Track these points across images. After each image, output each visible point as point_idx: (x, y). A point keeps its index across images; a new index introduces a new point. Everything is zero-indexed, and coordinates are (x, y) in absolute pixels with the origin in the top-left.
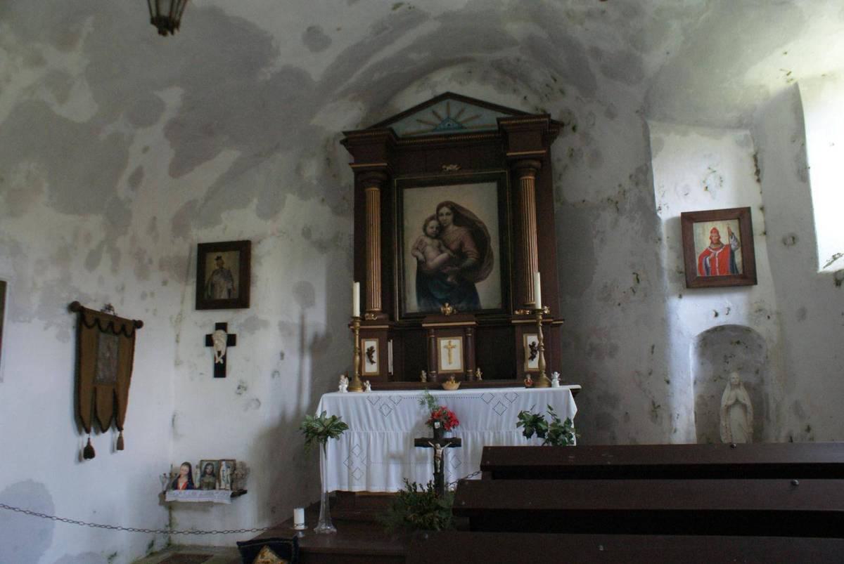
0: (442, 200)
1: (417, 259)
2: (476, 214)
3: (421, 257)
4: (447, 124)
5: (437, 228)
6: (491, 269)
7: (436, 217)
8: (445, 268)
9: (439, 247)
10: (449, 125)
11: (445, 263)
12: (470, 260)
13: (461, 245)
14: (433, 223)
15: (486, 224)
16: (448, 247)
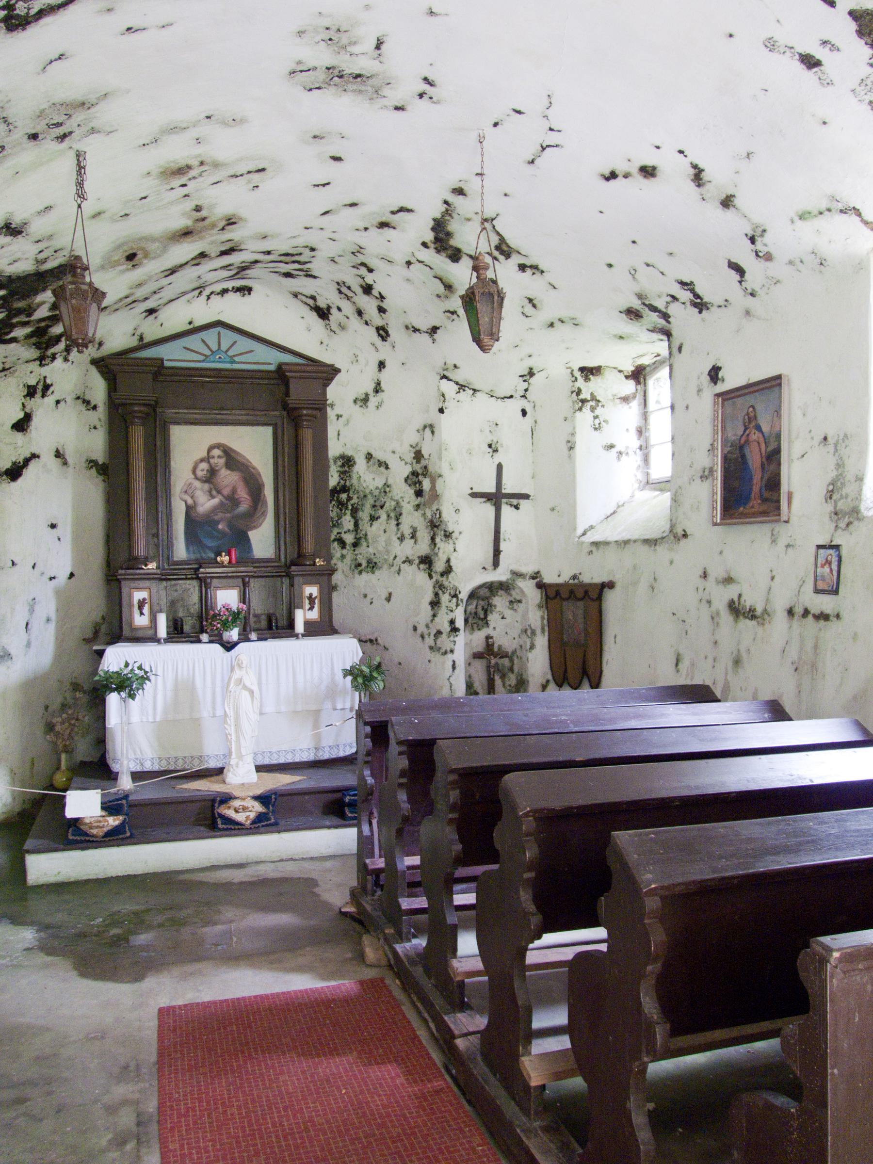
0: (214, 441)
1: (186, 503)
2: (248, 457)
3: (190, 501)
4: (217, 357)
7: (207, 459)
9: (210, 492)
10: (220, 358)
11: (214, 510)
12: (244, 507)
13: (234, 491)
14: (204, 466)
16: (219, 492)
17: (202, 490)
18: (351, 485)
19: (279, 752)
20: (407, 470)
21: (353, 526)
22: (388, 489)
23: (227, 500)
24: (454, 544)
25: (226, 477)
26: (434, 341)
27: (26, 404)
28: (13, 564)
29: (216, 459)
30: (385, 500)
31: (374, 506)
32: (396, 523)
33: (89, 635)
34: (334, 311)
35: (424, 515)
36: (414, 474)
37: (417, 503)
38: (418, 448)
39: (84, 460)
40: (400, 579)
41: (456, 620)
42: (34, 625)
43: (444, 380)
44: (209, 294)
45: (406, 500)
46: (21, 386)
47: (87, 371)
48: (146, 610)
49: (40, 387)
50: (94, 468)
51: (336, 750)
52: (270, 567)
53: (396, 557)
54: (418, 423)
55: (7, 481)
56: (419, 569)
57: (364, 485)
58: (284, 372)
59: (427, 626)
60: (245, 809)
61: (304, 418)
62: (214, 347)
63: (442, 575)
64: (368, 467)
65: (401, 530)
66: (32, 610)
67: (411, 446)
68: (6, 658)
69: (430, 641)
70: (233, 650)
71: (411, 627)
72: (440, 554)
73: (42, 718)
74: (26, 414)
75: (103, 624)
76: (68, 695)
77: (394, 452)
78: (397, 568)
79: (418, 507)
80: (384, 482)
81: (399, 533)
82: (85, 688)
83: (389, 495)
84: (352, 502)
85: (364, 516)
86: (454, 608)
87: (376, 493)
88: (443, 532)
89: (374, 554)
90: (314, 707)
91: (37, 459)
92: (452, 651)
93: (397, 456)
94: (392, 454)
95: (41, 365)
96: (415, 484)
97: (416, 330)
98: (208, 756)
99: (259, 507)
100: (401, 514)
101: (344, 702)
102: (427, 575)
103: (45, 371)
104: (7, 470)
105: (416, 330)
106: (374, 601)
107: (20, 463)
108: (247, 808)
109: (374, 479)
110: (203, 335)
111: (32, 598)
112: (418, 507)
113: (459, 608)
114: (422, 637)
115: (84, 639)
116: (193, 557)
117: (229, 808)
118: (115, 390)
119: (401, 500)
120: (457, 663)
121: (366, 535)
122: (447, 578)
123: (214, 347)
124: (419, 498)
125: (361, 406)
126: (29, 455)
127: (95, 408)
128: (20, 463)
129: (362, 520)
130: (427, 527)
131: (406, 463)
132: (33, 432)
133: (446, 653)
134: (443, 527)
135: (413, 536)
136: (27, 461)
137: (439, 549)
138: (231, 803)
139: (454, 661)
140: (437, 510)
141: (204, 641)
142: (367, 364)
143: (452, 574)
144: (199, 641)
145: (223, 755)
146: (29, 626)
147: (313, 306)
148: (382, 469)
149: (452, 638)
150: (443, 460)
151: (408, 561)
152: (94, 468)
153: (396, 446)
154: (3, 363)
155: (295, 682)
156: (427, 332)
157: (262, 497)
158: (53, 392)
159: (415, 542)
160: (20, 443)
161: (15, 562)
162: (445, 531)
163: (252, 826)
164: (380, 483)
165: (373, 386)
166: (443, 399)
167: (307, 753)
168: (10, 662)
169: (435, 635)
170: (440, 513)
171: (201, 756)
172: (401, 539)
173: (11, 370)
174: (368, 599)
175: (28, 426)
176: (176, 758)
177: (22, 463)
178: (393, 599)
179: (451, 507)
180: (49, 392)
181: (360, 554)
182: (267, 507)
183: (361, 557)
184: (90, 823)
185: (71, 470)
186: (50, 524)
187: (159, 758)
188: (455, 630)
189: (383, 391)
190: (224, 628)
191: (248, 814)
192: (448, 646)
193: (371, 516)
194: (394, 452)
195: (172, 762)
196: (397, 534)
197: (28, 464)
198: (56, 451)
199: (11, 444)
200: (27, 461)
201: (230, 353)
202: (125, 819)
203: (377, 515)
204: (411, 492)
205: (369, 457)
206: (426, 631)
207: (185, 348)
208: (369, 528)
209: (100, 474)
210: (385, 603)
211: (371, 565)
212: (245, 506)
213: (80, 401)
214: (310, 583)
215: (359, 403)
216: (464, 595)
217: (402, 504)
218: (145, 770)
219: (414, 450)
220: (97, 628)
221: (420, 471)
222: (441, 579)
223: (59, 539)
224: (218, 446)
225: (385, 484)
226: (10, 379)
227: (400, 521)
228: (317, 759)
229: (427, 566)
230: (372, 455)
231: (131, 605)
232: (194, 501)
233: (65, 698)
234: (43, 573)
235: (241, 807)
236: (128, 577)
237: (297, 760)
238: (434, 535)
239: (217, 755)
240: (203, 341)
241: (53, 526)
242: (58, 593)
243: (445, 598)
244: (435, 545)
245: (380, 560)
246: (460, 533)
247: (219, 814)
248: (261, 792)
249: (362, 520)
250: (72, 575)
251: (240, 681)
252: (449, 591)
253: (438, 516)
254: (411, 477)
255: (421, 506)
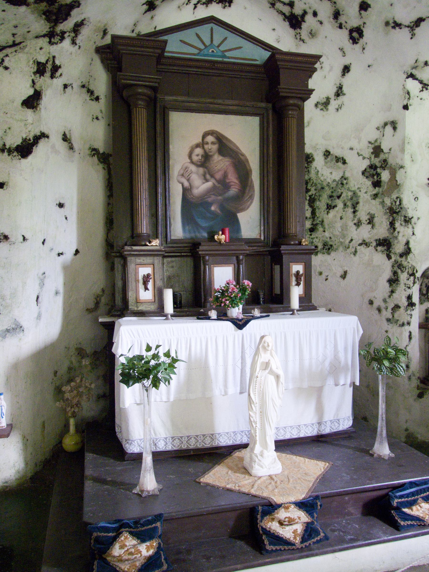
0: (207, 129)
1: (183, 186)
2: (238, 144)
3: (186, 184)
4: (210, 51)
5: (202, 156)
6: (253, 200)
7: (202, 145)
8: (210, 197)
9: (204, 175)
10: (213, 51)
11: (209, 192)
12: (233, 191)
13: (225, 175)
14: (199, 151)
15: (249, 158)
16: (212, 176)
17: (197, 173)
18: (310, 179)
19: (285, 428)
20: (365, 164)
21: (310, 214)
22: (345, 182)
23: (219, 184)
24: (413, 228)
25: (218, 162)
26: (413, 35)
27: (36, 81)
28: (24, 239)
29: (210, 145)
30: (342, 191)
31: (331, 197)
32: (352, 210)
33: (92, 305)
34: (309, 18)
35: (383, 203)
36: (372, 167)
37: (374, 192)
38: (376, 144)
39: (87, 146)
40: (356, 259)
41: (413, 296)
42: (43, 299)
43: (410, 79)
44: (196, 3)
45: (363, 191)
46: (31, 62)
47: (92, 60)
48: (150, 285)
49: (49, 66)
50: (96, 156)
51: (336, 424)
52: (256, 246)
53: (352, 240)
54: (379, 120)
55: (17, 158)
56: (377, 250)
57: (322, 178)
58: (276, 61)
59: (385, 301)
60: (291, 522)
61: (290, 108)
62: (207, 41)
63: (401, 256)
64: (326, 163)
65: (357, 217)
66: (42, 284)
67: (370, 143)
68: (18, 330)
69: (388, 314)
70: (244, 329)
71: (367, 301)
72: (400, 238)
73: (52, 383)
74: (36, 91)
75: (102, 296)
76: (73, 359)
77: (351, 149)
78: (353, 250)
79: (375, 196)
80: (341, 175)
81: (356, 219)
82: (88, 352)
83: (346, 187)
84: (310, 193)
85: (321, 204)
86: (412, 285)
87: (334, 185)
88: (403, 218)
89: (330, 238)
90: (318, 384)
91: (46, 139)
92: (409, 323)
93: (355, 152)
94: (351, 151)
95: (50, 42)
96: (373, 176)
97: (397, 25)
98: (219, 434)
99: (247, 191)
100: (358, 203)
101: (346, 378)
102: (385, 256)
103: (54, 50)
104: (18, 146)
105: (397, 25)
106: (329, 277)
107: (30, 140)
108: (293, 520)
109: (331, 173)
110: (198, 30)
111: (42, 272)
112: (375, 196)
113: (416, 285)
114: (379, 310)
115: (87, 310)
116: (188, 236)
117: (273, 519)
118: (120, 69)
119: (358, 191)
120: (413, 334)
121: (323, 221)
122: (406, 258)
123: (207, 41)
124: (377, 188)
125: (322, 110)
126: (39, 134)
127: (97, 99)
128: (30, 140)
129: (319, 209)
130: (385, 213)
131: (364, 158)
132: (43, 111)
133: (403, 325)
134: (403, 213)
135: (371, 221)
136: (37, 139)
137: (398, 232)
138: (276, 515)
139: (410, 333)
140: (397, 198)
141: (213, 318)
142: (331, 70)
143: (411, 255)
144: (209, 318)
145: (234, 432)
146: (40, 299)
147: (287, 14)
148: (340, 164)
149: (409, 312)
150: (406, 153)
151: (365, 243)
152: (96, 156)
153: (354, 143)
154: (14, 35)
155: (301, 359)
156: (408, 27)
157: (249, 182)
158: (61, 75)
159: (372, 227)
160: (30, 121)
161: (26, 237)
162: (405, 217)
163: (303, 545)
164: (337, 176)
165: (335, 90)
166: (407, 96)
167: (311, 428)
168: (21, 334)
169: (392, 309)
170: (400, 200)
171: (212, 435)
172: (358, 224)
173: (21, 45)
174: (324, 276)
175: (38, 104)
176: (188, 437)
177: (32, 141)
178: (348, 276)
179: (411, 195)
180: (58, 74)
181: (317, 238)
182: (254, 191)
183: (317, 240)
184: (120, 556)
185: (76, 155)
186: (58, 203)
187: (172, 438)
188: (411, 305)
189: (344, 94)
190: (231, 304)
191: (295, 527)
192: (405, 319)
193: (327, 205)
194: (351, 149)
195: (185, 440)
196: (354, 220)
197: (37, 143)
198: (63, 135)
199: (21, 120)
200: (37, 139)
201: (222, 48)
202: (159, 544)
203: (333, 204)
204: (368, 183)
205: (327, 154)
206: (383, 305)
207: (181, 41)
208: (325, 216)
209: (101, 163)
210: (341, 280)
211: (327, 247)
212: (234, 189)
213: (85, 90)
214: (297, 262)
215: (320, 107)
216: (418, 275)
217: (359, 194)
218: (158, 450)
219: (373, 146)
220: (98, 299)
221: (378, 165)
222: (399, 259)
223: (66, 218)
224: (212, 133)
225: (342, 177)
226: (21, 55)
227: (357, 209)
228: (320, 433)
229: (385, 248)
230: (329, 152)
231: (137, 281)
232: (190, 184)
233: (72, 363)
234: (52, 249)
235: (287, 519)
236: (133, 253)
237: (302, 435)
238: (394, 220)
239: (227, 433)
240: (197, 35)
241: (61, 205)
242: (66, 269)
243: (403, 277)
244: (394, 229)
245: (336, 242)
246: (418, 218)
247: (264, 530)
248: (303, 496)
249: (319, 209)
250: (77, 252)
251: (267, 365)
252: (407, 270)
253: (398, 203)
254: (368, 170)
255: (379, 195)
